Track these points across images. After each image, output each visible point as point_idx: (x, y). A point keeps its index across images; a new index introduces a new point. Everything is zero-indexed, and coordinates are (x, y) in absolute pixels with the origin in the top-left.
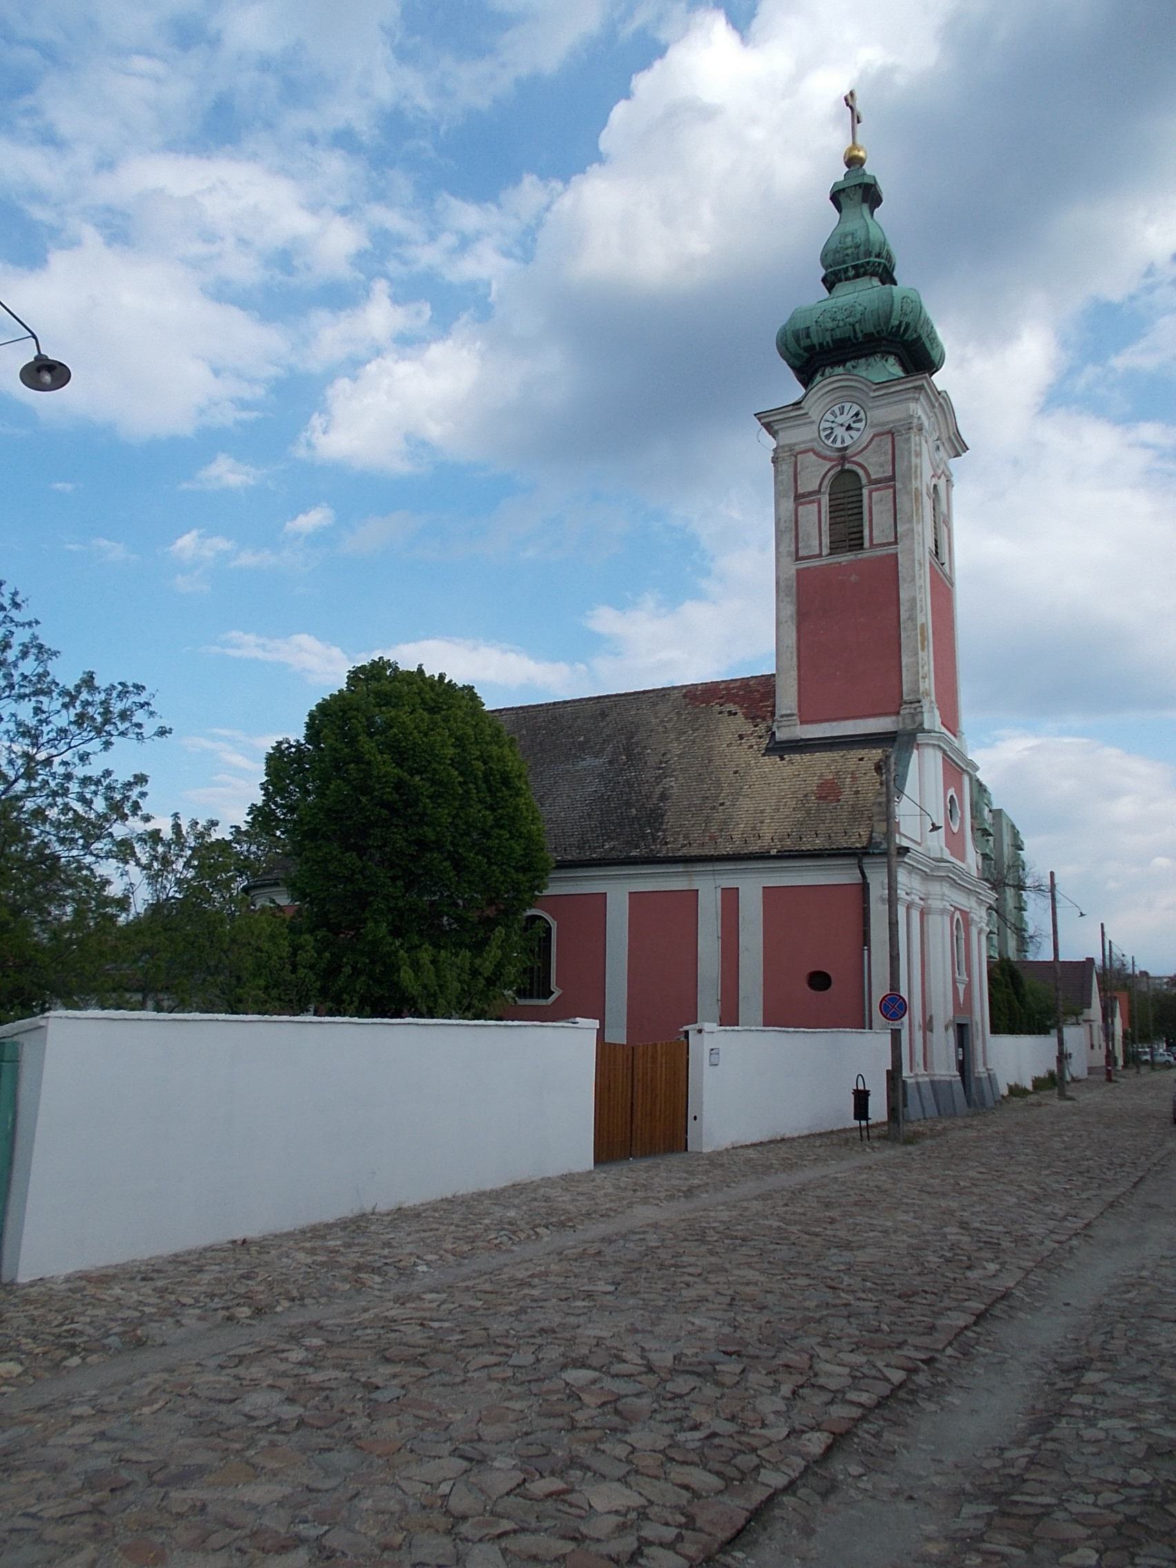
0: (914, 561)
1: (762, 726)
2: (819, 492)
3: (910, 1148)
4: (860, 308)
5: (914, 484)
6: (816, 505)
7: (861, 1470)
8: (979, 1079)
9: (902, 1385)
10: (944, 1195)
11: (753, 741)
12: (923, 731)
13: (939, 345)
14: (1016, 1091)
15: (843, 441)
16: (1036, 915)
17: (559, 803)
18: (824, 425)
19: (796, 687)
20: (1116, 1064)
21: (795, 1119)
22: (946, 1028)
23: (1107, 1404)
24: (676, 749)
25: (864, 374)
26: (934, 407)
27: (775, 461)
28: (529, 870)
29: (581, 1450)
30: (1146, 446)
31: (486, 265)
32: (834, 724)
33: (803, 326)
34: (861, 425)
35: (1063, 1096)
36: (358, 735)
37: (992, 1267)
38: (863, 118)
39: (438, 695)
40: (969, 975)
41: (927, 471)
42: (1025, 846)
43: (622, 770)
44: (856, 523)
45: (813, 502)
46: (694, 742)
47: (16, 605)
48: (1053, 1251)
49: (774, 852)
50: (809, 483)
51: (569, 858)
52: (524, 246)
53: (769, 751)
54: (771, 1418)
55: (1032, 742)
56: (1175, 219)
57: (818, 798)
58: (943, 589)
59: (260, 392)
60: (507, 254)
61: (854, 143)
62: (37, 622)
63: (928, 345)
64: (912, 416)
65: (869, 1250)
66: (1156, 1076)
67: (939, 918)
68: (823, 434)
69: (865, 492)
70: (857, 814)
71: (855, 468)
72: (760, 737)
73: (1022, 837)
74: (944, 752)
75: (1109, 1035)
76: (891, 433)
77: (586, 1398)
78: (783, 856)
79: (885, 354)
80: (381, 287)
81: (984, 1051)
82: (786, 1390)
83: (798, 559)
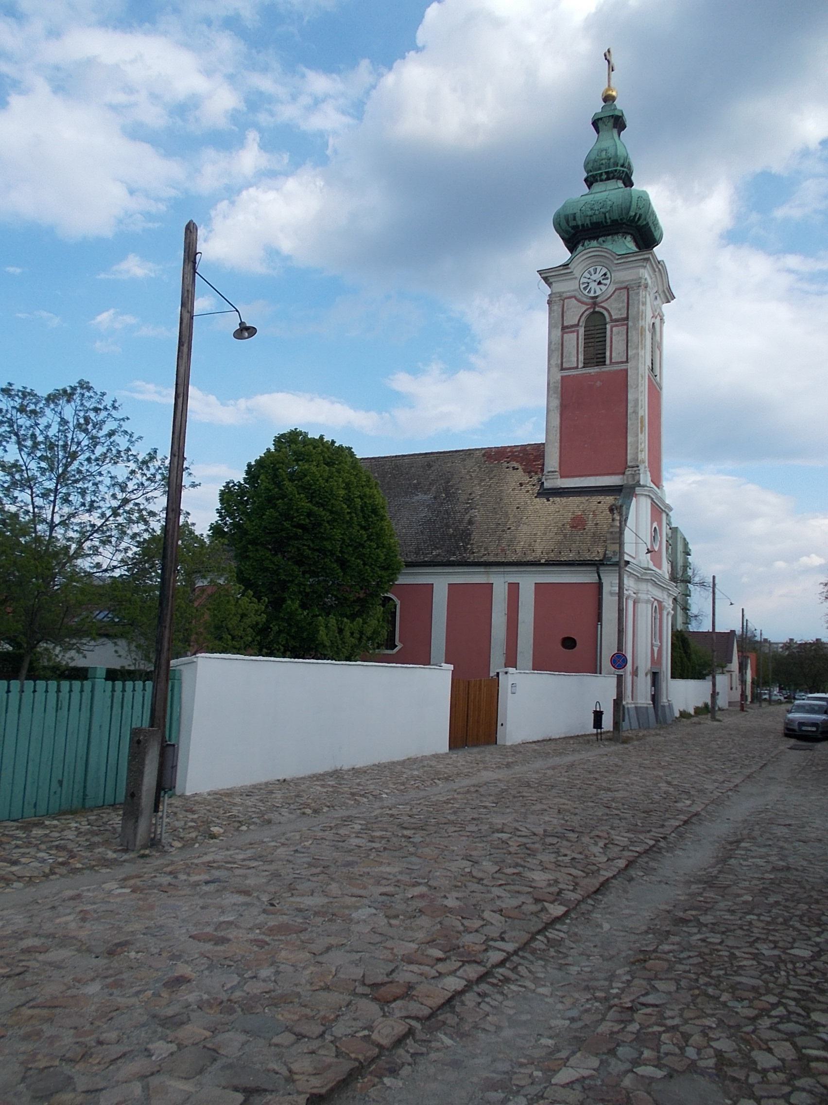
0: (638, 374)
1: (535, 478)
2: (578, 325)
3: (626, 746)
4: (609, 203)
5: (641, 323)
6: (575, 334)
7: (642, 874)
8: (663, 706)
9: (654, 846)
10: (654, 768)
11: (529, 488)
12: (640, 486)
13: (660, 228)
14: (684, 715)
15: (595, 292)
16: (699, 601)
17: (404, 523)
18: (583, 280)
19: (558, 454)
20: (746, 700)
21: (557, 729)
22: (646, 675)
23: (752, 854)
24: (478, 490)
25: (610, 247)
26: (655, 271)
27: (549, 302)
28: (387, 569)
29: (519, 861)
30: (790, 271)
31: (329, 120)
32: (582, 479)
33: (572, 212)
34: (607, 282)
35: (714, 719)
36: (283, 480)
37: (688, 802)
38: (615, 68)
39: (332, 454)
40: (661, 642)
41: (649, 314)
42: (692, 553)
43: (442, 503)
44: (601, 347)
45: (573, 332)
46: (490, 486)
47: (114, 408)
48: (719, 797)
49: (543, 561)
50: (572, 319)
51: (410, 560)
52: (357, 109)
53: (539, 495)
54: (597, 854)
55: (698, 478)
56: (827, 109)
57: (572, 527)
58: (655, 392)
59: (162, 207)
60: (344, 113)
61: (609, 86)
62: (128, 419)
63: (653, 229)
64: (641, 278)
65: (621, 792)
66: (772, 709)
67: (644, 605)
68: (582, 287)
69: (608, 326)
70: (596, 538)
71: (602, 310)
72: (534, 485)
73: (690, 546)
74: (652, 499)
75: (743, 682)
76: (627, 288)
77: (511, 843)
78: (549, 564)
79: (625, 234)
80: (253, 136)
81: (667, 689)
82: (601, 844)
83: (562, 369)
